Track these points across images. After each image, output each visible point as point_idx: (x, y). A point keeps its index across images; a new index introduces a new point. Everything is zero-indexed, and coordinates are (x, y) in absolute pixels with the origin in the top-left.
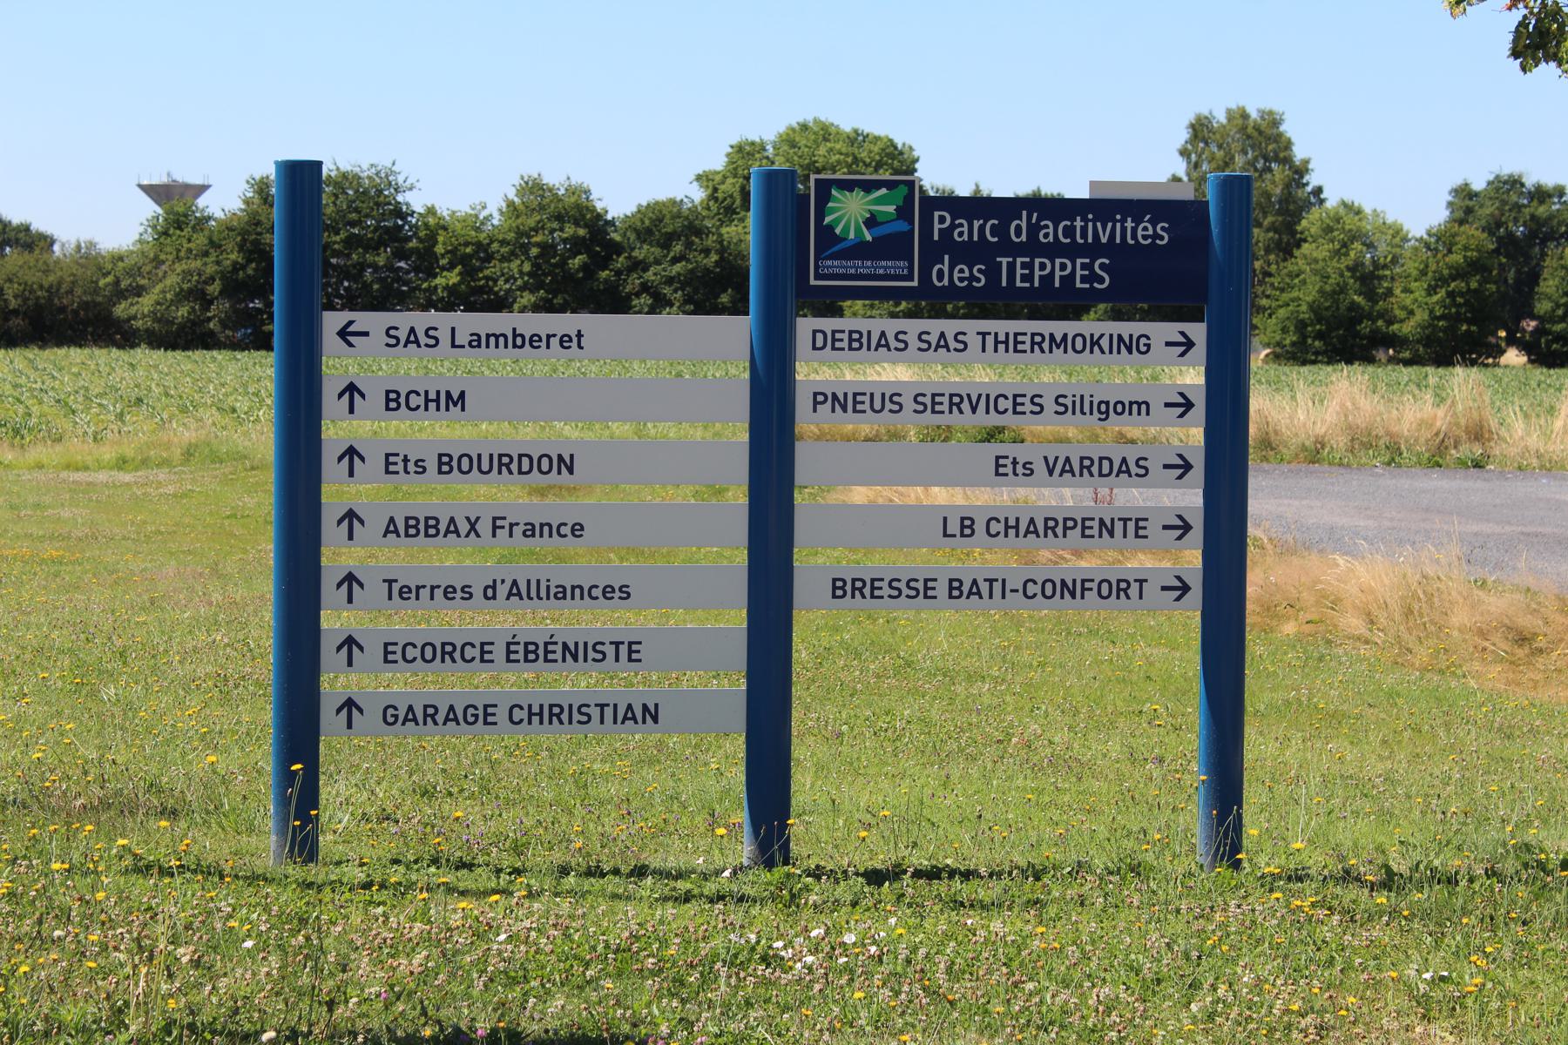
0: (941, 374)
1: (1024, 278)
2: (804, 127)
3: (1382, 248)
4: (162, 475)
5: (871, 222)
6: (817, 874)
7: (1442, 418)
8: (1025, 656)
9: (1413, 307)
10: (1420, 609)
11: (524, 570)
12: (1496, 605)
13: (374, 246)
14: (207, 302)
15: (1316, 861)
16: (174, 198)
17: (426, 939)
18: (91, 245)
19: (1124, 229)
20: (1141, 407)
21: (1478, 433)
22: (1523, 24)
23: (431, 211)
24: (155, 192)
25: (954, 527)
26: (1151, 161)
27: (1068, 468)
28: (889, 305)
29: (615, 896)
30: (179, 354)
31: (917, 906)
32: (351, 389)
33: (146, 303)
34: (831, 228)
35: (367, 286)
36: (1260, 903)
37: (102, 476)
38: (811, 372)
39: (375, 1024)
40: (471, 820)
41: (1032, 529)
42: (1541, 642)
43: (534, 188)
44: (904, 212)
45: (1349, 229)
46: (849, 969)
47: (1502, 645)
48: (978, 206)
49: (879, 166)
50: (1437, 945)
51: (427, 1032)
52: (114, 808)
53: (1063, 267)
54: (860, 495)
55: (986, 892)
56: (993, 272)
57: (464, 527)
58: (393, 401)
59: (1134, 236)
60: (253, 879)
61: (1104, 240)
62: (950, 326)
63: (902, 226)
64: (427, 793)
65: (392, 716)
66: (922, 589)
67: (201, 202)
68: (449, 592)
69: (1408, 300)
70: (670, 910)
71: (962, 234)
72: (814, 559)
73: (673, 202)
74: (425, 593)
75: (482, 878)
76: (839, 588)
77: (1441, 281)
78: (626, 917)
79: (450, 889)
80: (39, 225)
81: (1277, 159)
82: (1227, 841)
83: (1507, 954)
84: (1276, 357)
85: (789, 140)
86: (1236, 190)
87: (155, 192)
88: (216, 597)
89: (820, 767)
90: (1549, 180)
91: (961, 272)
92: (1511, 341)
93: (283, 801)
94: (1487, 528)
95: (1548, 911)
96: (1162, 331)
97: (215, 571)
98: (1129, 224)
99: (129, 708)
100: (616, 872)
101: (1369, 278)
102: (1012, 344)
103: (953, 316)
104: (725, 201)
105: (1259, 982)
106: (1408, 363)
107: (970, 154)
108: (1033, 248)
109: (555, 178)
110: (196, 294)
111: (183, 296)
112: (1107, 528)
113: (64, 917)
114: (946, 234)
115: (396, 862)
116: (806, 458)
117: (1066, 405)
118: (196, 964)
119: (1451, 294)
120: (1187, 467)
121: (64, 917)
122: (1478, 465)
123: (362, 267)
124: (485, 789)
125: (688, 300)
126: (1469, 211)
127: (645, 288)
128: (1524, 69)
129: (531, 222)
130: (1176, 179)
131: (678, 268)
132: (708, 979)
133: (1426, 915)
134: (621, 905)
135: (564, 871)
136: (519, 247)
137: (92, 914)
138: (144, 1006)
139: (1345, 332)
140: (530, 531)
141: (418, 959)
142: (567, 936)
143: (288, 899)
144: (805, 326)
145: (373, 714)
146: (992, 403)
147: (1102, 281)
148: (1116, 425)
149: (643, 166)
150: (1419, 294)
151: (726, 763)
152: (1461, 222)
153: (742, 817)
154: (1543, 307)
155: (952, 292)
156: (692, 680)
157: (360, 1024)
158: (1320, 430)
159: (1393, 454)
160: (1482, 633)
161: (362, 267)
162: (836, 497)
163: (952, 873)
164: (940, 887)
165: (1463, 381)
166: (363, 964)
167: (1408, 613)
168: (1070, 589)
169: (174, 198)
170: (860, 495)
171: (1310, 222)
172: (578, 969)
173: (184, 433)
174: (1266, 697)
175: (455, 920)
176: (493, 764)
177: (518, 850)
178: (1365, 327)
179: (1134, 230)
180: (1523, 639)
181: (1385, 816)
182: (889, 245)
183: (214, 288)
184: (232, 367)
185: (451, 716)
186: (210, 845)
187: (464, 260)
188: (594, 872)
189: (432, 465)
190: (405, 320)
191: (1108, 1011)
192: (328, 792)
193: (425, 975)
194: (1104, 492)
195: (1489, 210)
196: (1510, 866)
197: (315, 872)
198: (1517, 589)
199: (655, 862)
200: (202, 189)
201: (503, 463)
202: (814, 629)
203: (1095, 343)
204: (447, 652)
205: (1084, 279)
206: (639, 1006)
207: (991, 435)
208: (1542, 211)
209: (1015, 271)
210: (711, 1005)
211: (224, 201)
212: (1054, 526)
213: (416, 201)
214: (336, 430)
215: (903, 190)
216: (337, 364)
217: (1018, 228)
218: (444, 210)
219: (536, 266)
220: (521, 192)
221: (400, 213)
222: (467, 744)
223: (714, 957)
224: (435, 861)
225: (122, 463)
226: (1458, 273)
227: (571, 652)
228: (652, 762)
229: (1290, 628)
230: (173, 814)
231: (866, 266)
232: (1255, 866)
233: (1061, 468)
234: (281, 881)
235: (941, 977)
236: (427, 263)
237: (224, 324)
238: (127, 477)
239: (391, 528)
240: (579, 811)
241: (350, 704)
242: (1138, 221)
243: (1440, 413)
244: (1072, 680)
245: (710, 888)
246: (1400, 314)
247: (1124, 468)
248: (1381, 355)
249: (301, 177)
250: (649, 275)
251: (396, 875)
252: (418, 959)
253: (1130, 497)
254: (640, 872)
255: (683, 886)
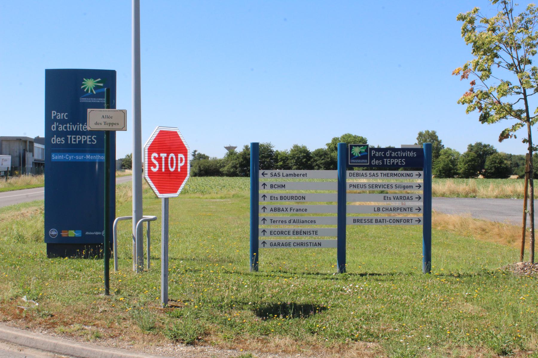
0: (373, 181)
1: (74, 141)
2: (346, 135)
3: (455, 156)
4: (229, 200)
5: (360, 153)
6: (351, 274)
7: (467, 188)
8: (389, 233)
9: (461, 167)
10: (463, 224)
11: (295, 217)
12: (479, 224)
13: (267, 158)
14: (237, 168)
15: (446, 272)
16: (231, 150)
17: (278, 286)
18: (216, 158)
19: (79, 127)
20: (411, 187)
21: (474, 191)
22: (482, 115)
23: (277, 151)
24: (227, 148)
25: (376, 209)
26: (411, 140)
27: (397, 198)
28: (361, 168)
29: (313, 278)
30: (231, 178)
31: (370, 280)
32: (264, 184)
33: (226, 169)
34: (352, 154)
35: (265, 165)
36: (436, 281)
37: (218, 200)
38: (349, 181)
39: (269, 301)
40: (286, 264)
41: (391, 210)
42: (487, 230)
43: (296, 146)
44: (366, 151)
45: (448, 153)
46: (357, 292)
47: (479, 231)
48: (379, 150)
49: (360, 142)
50: (469, 288)
51: (279, 303)
52: (222, 261)
53: (84, 138)
54: (357, 203)
55: (382, 278)
56: (383, 162)
57: (285, 210)
58: (272, 186)
59: (82, 129)
60: (247, 274)
61: (74, 130)
62: (375, 172)
63: (366, 153)
64: (278, 259)
65: (272, 245)
66: (370, 221)
67: (235, 150)
68: (282, 222)
69: (460, 166)
70: (324, 281)
71: (377, 154)
72: (350, 216)
73: (322, 149)
74: (278, 222)
75: (288, 275)
76: (355, 221)
77: (467, 162)
78: (316, 282)
79: (283, 277)
80: (206, 154)
81: (435, 140)
82: (428, 269)
83: (482, 290)
84: (435, 177)
85: (343, 137)
86: (429, 146)
87: (227, 148)
88: (239, 222)
89: (351, 254)
90: (487, 144)
91: (377, 162)
92: (480, 174)
93: (252, 260)
94: (476, 209)
95: (490, 281)
96: (415, 173)
97: (238, 217)
98: (81, 125)
99: (224, 243)
100: (313, 274)
101: (453, 162)
102: (387, 175)
103: (374, 170)
104: (333, 147)
105: (434, 296)
106: (461, 178)
107: (376, 141)
108: (391, 157)
109: (300, 145)
110: (235, 167)
111: (232, 167)
112: (405, 209)
113: (213, 281)
114: (374, 155)
115: (272, 271)
116: (348, 196)
117: (396, 186)
118: (237, 290)
119: (469, 165)
120: (420, 198)
121: (213, 281)
122: (474, 197)
123: (264, 161)
124: (288, 258)
125: (325, 167)
126: (472, 149)
127: (317, 165)
128: (482, 123)
129: (296, 153)
130: (416, 144)
131: (323, 161)
132: (331, 294)
133: (466, 283)
134: (314, 280)
135: (304, 273)
136: (293, 158)
137: (218, 281)
138: (227, 298)
139: (449, 172)
140: (297, 210)
141: (277, 289)
142: (304, 286)
143: (253, 278)
144: (348, 172)
145: (268, 244)
146: (383, 186)
147: (94, 142)
148: (406, 190)
149: (317, 142)
150: (463, 165)
151: (334, 253)
152: (470, 151)
153: (337, 264)
154: (486, 167)
155: (375, 165)
156: (326, 238)
157: (267, 301)
158: (444, 191)
159: (458, 195)
160: (476, 229)
161: (264, 161)
162: (353, 204)
163: (376, 274)
164: (374, 277)
165: (471, 181)
166: (267, 290)
167: (462, 225)
168: (398, 221)
169: (231, 150)
170: (357, 203)
171: (442, 152)
172: (306, 292)
173: (233, 192)
174: (435, 241)
175: (284, 282)
176: (290, 254)
177: (295, 269)
178: (452, 171)
179: (82, 127)
180: (484, 230)
181: (458, 264)
182: (363, 157)
183: (238, 166)
184: (241, 180)
185: (283, 245)
186: (239, 268)
187: (283, 160)
188: (309, 274)
189: (279, 198)
190: (274, 171)
191: (406, 301)
192: (260, 258)
193: (278, 293)
194: (403, 203)
195: (475, 149)
196: (482, 273)
197: (258, 273)
198: (482, 220)
199: (321, 272)
200: (236, 147)
201: (292, 198)
202: (350, 228)
203: (402, 175)
204: (282, 233)
205: (90, 141)
206: (318, 298)
207: (382, 192)
208: (485, 149)
209: (387, 162)
210: (331, 299)
211: (239, 150)
212: (395, 209)
213: (274, 149)
214: (261, 192)
215: (366, 147)
216: (261, 180)
217: (54, 127)
218: (279, 151)
219: (296, 161)
220: (294, 147)
221: (271, 151)
222: (286, 250)
223: (332, 290)
224: (280, 271)
225: (221, 198)
226: (470, 161)
227: (305, 233)
228: (320, 253)
229: (439, 228)
230: (232, 262)
231: (359, 161)
232: (434, 273)
233: (396, 198)
234: (252, 275)
235: (374, 294)
236: (276, 161)
237: (240, 172)
238: (222, 200)
239: (271, 210)
240: (306, 262)
241: (264, 242)
242: (410, 152)
243: (467, 187)
244: (398, 238)
245: (331, 277)
246: (459, 169)
247: (408, 198)
248: (455, 176)
249: (255, 146)
250: (318, 162)
251: (273, 274)
252: (277, 289)
253: (409, 204)
254: (318, 274)
255: (326, 276)
